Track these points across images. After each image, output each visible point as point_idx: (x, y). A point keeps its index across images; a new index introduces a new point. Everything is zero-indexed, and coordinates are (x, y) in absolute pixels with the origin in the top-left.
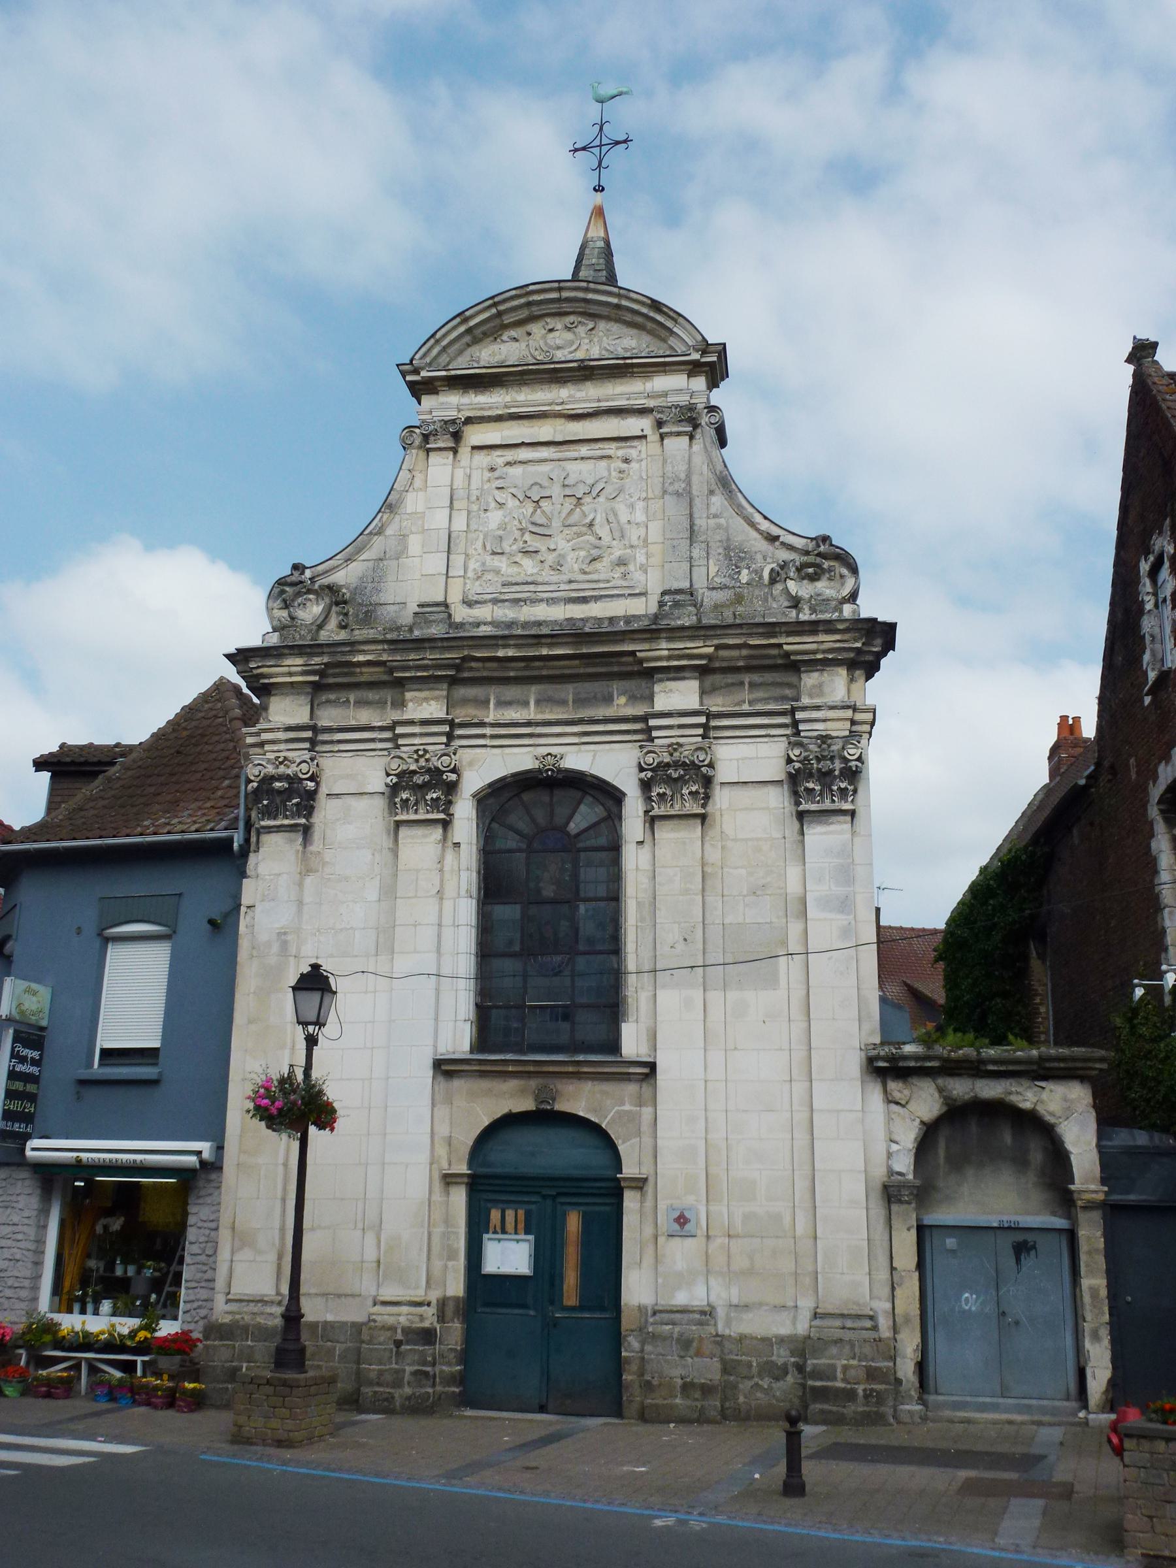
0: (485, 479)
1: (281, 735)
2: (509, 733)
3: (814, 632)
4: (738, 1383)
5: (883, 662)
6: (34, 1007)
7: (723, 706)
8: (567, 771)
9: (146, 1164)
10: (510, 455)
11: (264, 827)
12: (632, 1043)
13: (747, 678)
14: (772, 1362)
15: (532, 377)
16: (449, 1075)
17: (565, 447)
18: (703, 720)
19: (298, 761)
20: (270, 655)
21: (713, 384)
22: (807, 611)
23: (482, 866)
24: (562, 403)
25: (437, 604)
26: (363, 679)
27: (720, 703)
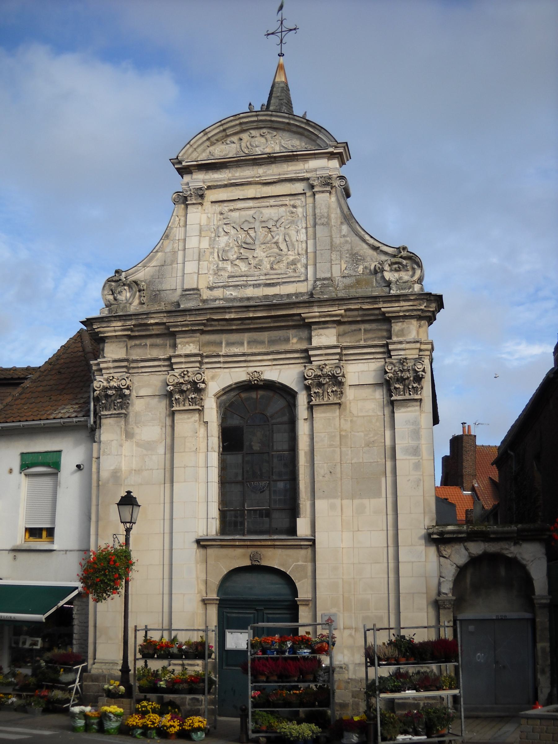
0: (218, 219)
1: (111, 365)
3: (398, 301)
4: (359, 702)
5: (438, 316)
7: (350, 342)
8: (265, 380)
10: (232, 205)
11: (103, 415)
13: (363, 327)
15: (242, 163)
16: (205, 547)
18: (338, 350)
19: (120, 378)
20: (104, 321)
21: (342, 163)
22: (394, 288)
23: (220, 434)
24: (259, 177)
25: (193, 289)
26: (153, 333)
27: (348, 341)
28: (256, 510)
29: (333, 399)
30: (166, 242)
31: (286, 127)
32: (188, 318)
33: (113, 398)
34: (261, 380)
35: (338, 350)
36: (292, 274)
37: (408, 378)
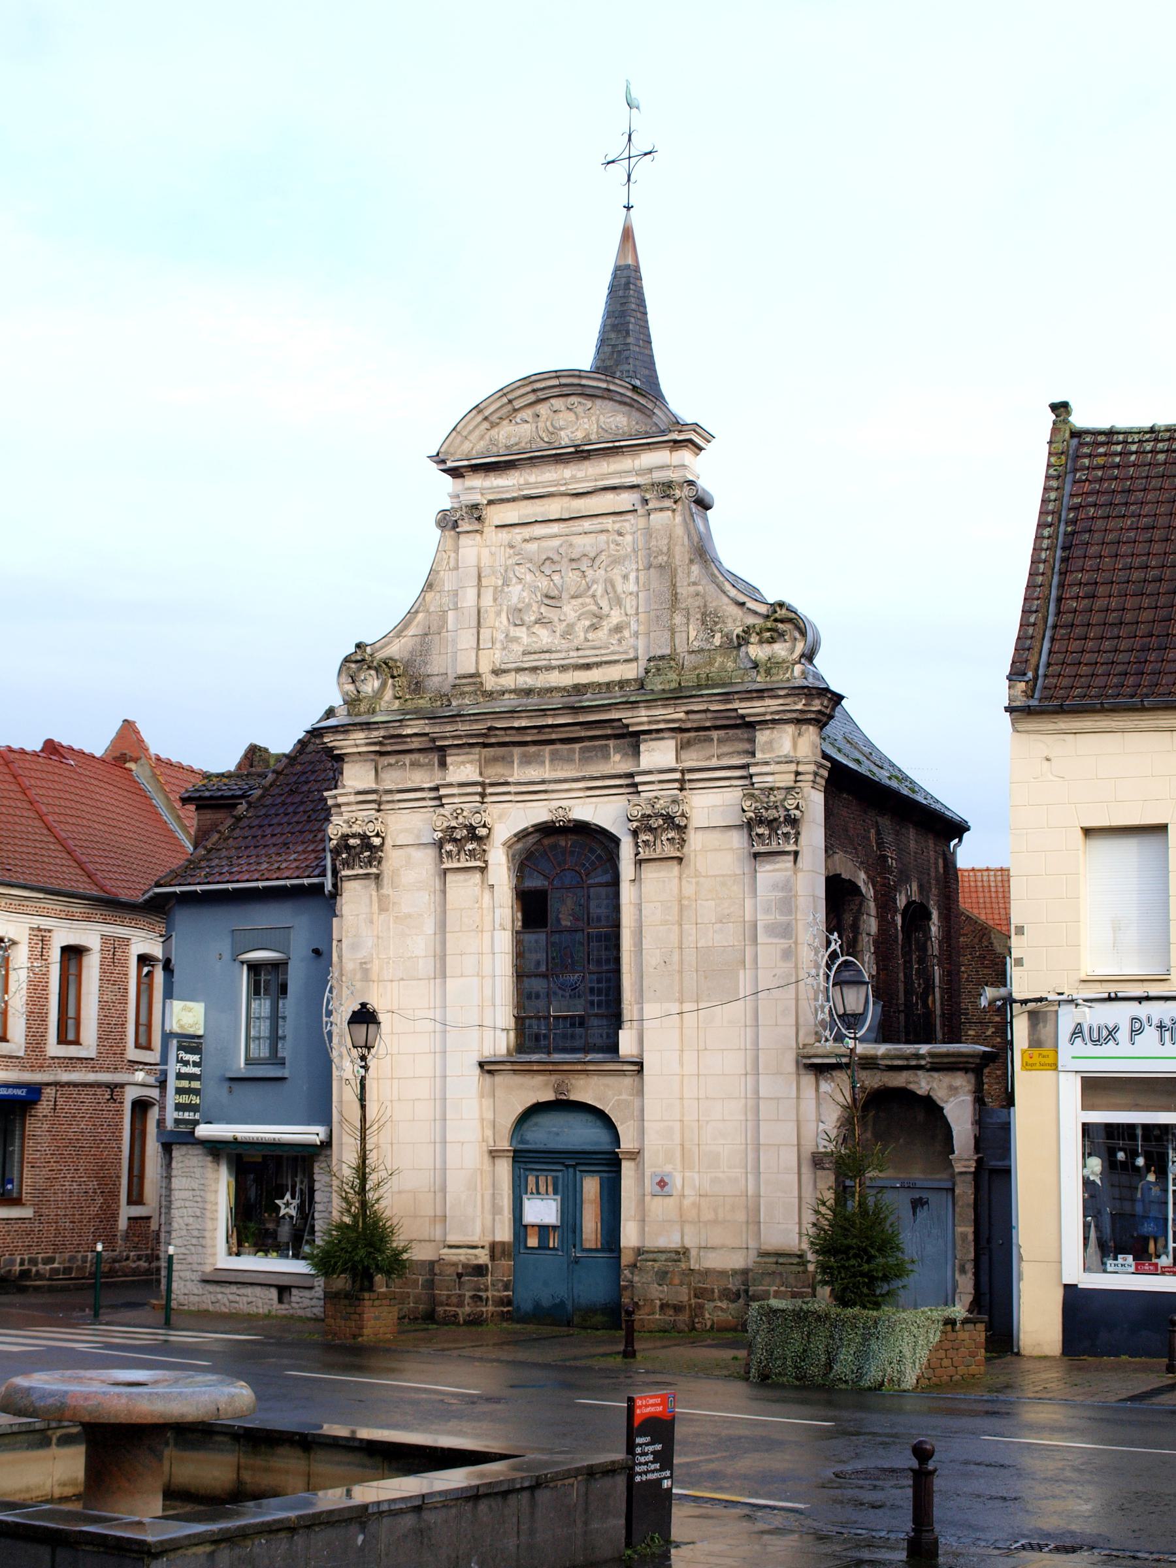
0: (507, 555)
1: (352, 798)
2: (533, 791)
3: (762, 698)
6: (191, 1021)
7: (697, 760)
8: (575, 821)
9: (282, 1142)
10: (527, 532)
12: (627, 1042)
13: (715, 734)
14: (729, 1289)
17: (571, 523)
19: (367, 820)
25: (471, 676)
26: (413, 746)
28: (565, 1017)
29: (670, 851)
30: (429, 596)
31: (606, 394)
32: (460, 726)
33: (358, 850)
34: (569, 821)
35: (678, 776)
36: (616, 648)
37: (775, 819)
